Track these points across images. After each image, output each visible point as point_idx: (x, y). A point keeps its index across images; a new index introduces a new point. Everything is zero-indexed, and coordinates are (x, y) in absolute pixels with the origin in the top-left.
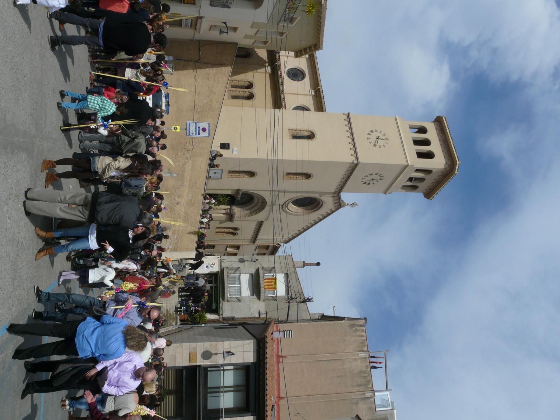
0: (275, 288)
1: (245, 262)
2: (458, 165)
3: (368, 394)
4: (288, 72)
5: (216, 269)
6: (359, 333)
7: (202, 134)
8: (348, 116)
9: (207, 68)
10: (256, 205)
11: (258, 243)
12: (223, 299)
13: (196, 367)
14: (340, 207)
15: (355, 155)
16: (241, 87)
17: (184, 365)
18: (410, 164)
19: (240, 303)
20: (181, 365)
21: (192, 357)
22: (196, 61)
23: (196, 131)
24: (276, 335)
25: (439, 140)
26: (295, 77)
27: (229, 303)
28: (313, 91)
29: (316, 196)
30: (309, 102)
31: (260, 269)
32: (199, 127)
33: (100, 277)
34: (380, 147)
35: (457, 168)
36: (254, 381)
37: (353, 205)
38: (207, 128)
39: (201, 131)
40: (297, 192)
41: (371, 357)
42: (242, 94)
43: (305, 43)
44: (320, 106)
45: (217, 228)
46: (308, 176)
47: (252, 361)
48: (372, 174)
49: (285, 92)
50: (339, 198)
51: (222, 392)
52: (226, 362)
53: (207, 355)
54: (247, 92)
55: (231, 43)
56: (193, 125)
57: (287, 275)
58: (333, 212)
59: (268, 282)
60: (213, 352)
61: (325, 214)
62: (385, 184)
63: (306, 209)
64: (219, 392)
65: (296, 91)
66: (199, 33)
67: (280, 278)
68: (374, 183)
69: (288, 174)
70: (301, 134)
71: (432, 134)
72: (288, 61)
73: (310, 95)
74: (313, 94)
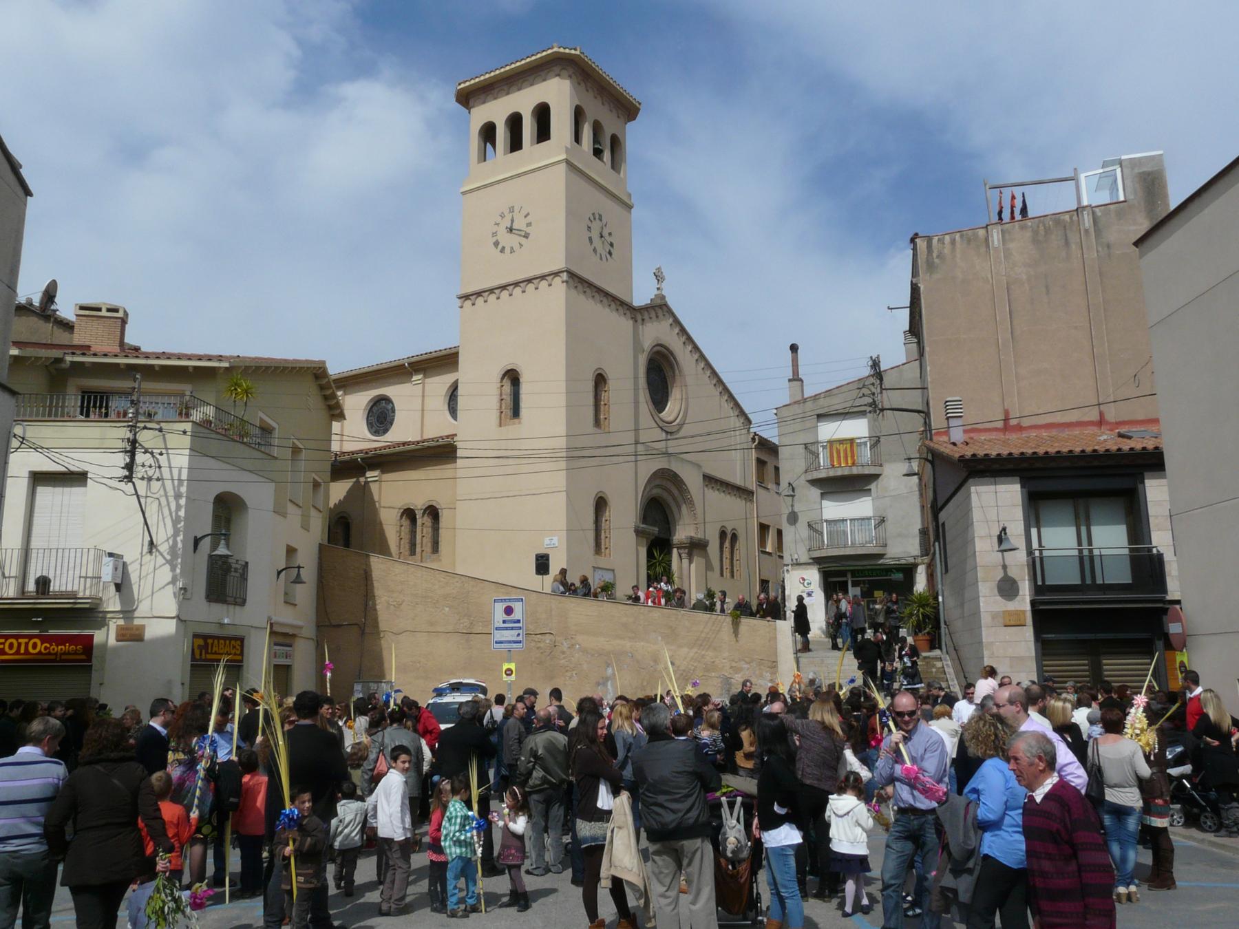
0: (852, 441)
2: (562, 50)
5: (813, 576)
6: (947, 251)
7: (517, 615)
8: (466, 297)
10: (670, 492)
11: (752, 484)
12: (881, 556)
13: (1036, 613)
14: (666, 305)
15: (549, 278)
16: (413, 533)
17: (1032, 638)
18: (564, 156)
19: (885, 518)
21: (1012, 622)
22: (363, 633)
23: (512, 628)
24: (957, 435)
25: (508, 93)
27: (889, 542)
28: (415, 378)
29: (643, 360)
30: (438, 384)
31: (810, 478)
32: (504, 622)
34: (529, 225)
35: (567, 51)
41: (1000, 219)
42: (428, 531)
43: (314, 400)
44: (446, 361)
45: (722, 575)
46: (600, 380)
47: (1017, 487)
48: (590, 239)
49: (419, 439)
50: (646, 309)
51: (1091, 551)
52: (1020, 543)
53: (1008, 588)
54: (423, 521)
55: (320, 558)
56: (499, 635)
58: (677, 321)
59: (839, 457)
60: (1000, 574)
61: (683, 339)
63: (678, 383)
64: (1091, 558)
65: (417, 414)
66: (301, 627)
67: (829, 431)
68: (610, 234)
69: (597, 422)
70: (508, 399)
71: (497, 110)
72: (352, 434)
73: (423, 383)
74: (420, 377)
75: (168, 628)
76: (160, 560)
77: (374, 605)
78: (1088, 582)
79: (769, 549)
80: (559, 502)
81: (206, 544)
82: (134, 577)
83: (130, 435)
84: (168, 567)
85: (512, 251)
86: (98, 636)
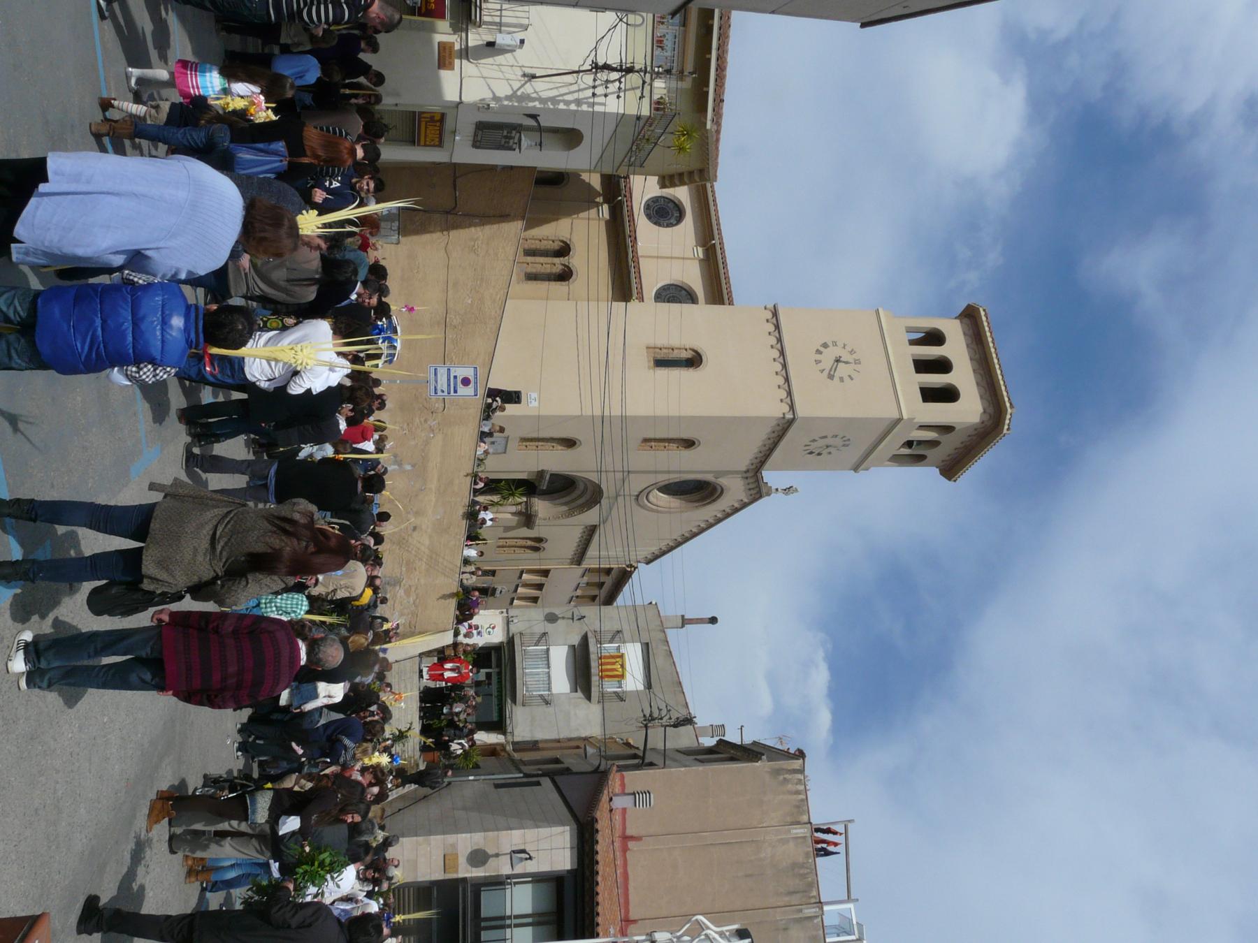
0: (622, 676)
1: (560, 621)
3: (810, 911)
4: (648, 207)
5: (497, 637)
7: (462, 390)
8: (775, 313)
9: (470, 226)
10: (580, 496)
11: (586, 564)
12: (514, 701)
14: (761, 497)
17: (433, 878)
18: (905, 416)
19: (550, 709)
20: (427, 878)
21: (448, 861)
23: (449, 385)
24: (619, 802)
26: (662, 216)
27: (527, 709)
28: (700, 249)
29: (709, 478)
30: (693, 277)
31: (590, 635)
32: (455, 377)
33: (278, 371)
34: (842, 379)
36: (572, 898)
37: (788, 490)
38: (472, 379)
39: (460, 385)
40: (669, 472)
42: (548, 269)
46: (689, 444)
47: (568, 867)
49: (640, 253)
51: (509, 926)
52: (519, 869)
53: (478, 857)
54: (557, 264)
56: (442, 372)
57: (646, 648)
58: (744, 505)
60: (490, 851)
61: (728, 510)
62: (855, 454)
64: (503, 927)
65: (665, 252)
67: (633, 654)
71: (956, 348)
72: (644, 188)
74: (701, 256)
75: (451, 94)
76: (516, 85)
77: (475, 225)
78: (483, 924)
79: (525, 576)
80: (574, 411)
81: (532, 123)
82: (500, 59)
83: (637, 67)
84: (510, 92)
85: (818, 362)
86: (443, 25)
